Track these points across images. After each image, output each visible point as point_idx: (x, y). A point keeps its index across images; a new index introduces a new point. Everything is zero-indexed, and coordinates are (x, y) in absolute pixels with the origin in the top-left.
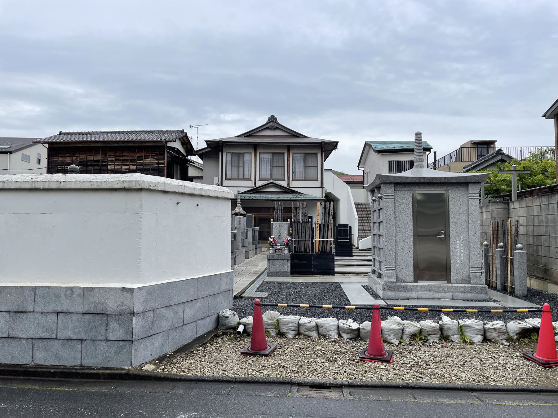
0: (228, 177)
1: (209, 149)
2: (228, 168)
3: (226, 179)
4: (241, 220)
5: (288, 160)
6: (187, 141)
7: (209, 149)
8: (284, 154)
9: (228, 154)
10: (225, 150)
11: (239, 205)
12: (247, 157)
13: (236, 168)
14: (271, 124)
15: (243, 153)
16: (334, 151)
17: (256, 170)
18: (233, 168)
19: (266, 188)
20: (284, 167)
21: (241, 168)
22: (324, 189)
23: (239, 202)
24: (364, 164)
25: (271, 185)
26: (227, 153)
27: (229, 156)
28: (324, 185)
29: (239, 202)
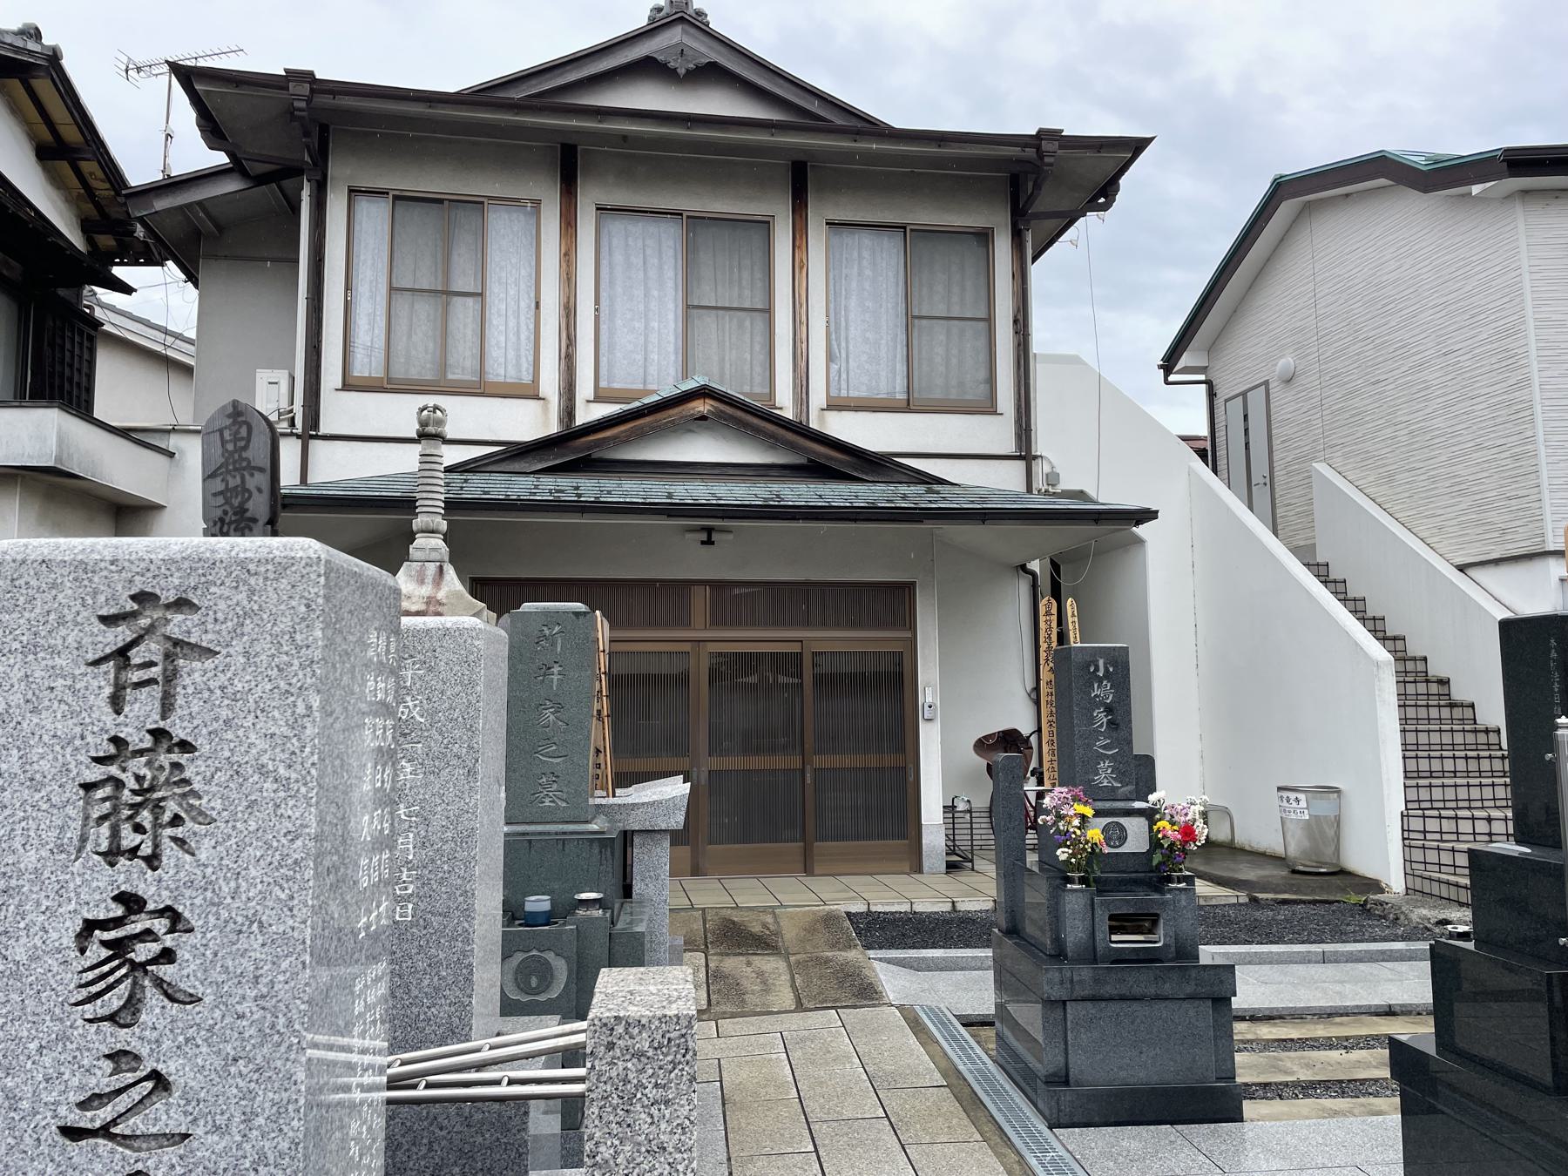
0: (360, 369)
1: (231, 186)
2: (363, 289)
3: (348, 385)
4: (236, 715)
5: (799, 267)
6: (71, 134)
7: (231, 186)
8: (765, 226)
9: (365, 207)
10: (342, 172)
11: (429, 546)
12: (504, 229)
13: (425, 310)
14: (675, 35)
15: (477, 204)
16: (1089, 224)
17: (578, 318)
18: (402, 303)
19: (641, 436)
20: (768, 311)
21: (464, 311)
22: (1040, 470)
23: (431, 516)
24: (1212, 349)
25: (702, 407)
26: (353, 192)
27: (374, 215)
28: (1042, 444)
29: (431, 516)
